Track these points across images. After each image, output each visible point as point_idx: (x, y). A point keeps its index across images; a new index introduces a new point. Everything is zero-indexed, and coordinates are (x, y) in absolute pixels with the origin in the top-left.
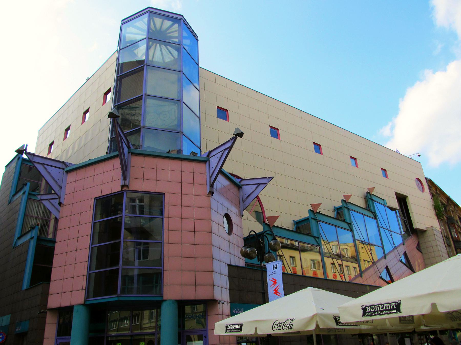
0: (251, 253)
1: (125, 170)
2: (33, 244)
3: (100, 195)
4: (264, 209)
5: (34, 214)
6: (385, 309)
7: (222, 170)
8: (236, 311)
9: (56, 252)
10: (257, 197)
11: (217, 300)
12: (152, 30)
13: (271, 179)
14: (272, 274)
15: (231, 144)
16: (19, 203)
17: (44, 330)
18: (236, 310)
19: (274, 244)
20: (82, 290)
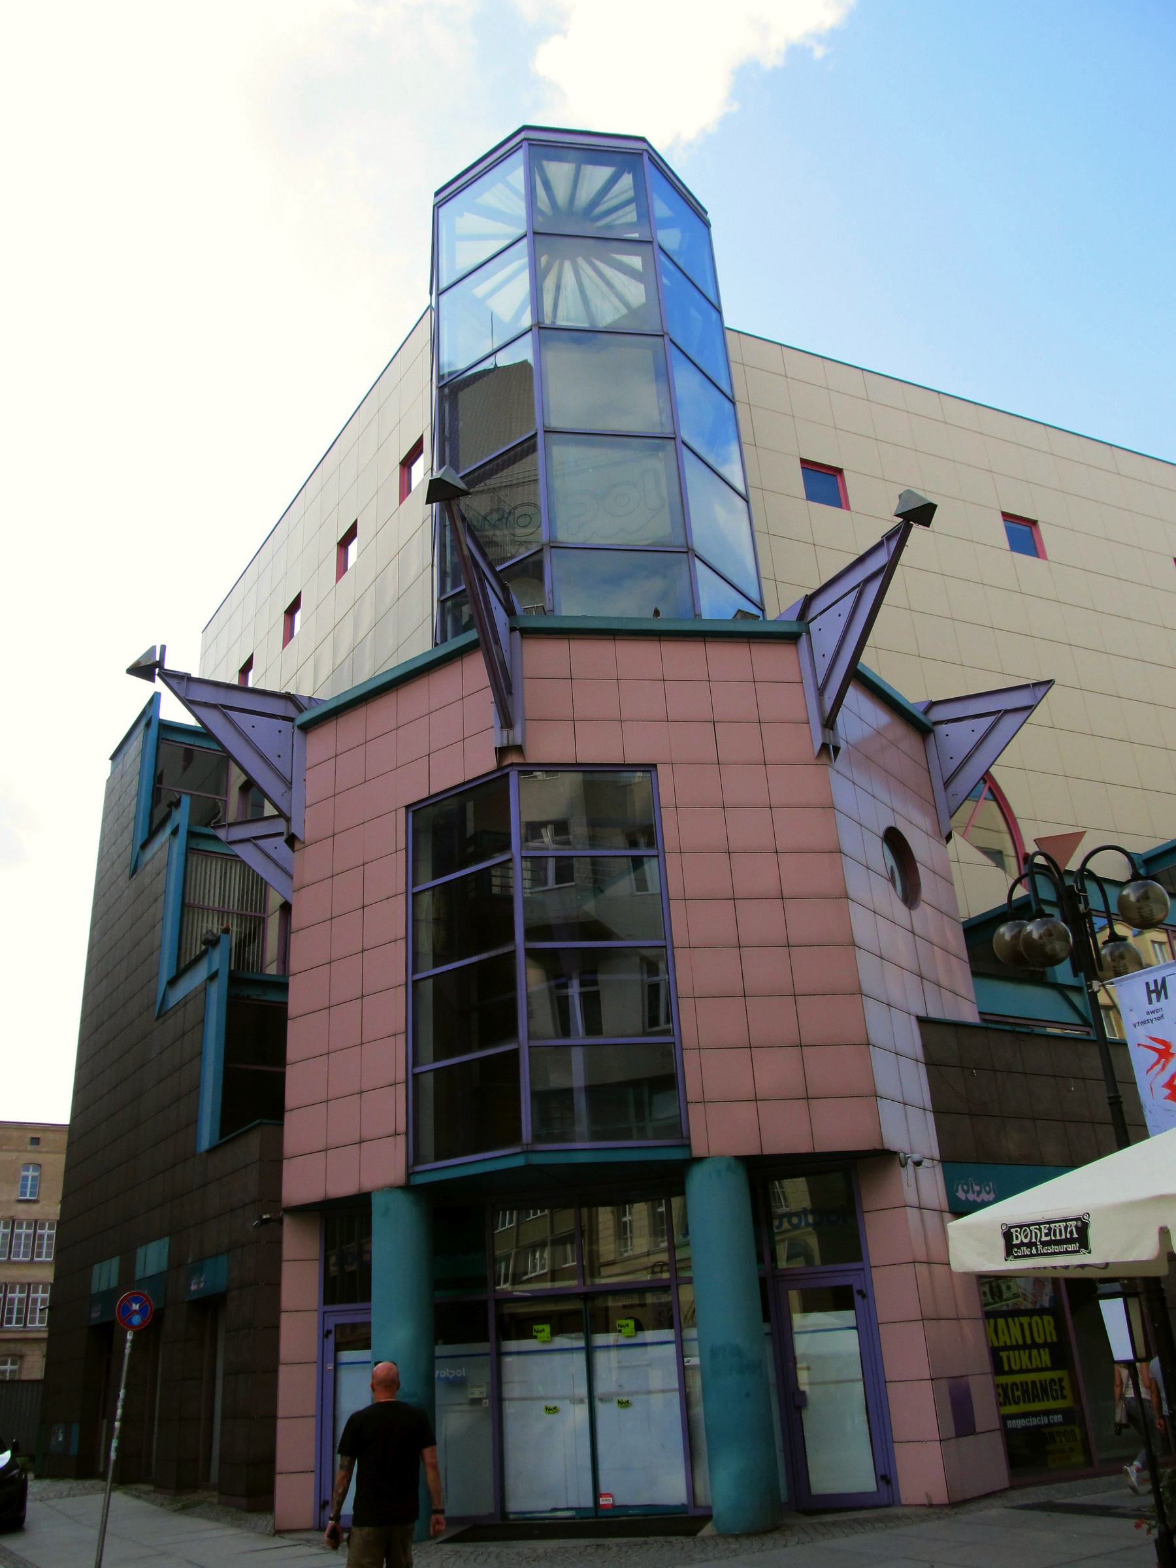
0: (1045, 939)
1: (505, 692)
2: (217, 994)
3: (425, 795)
4: (1014, 819)
5: (214, 902)
6: (1053, 1238)
7: (859, 667)
8: (966, 1192)
9: (292, 1010)
10: (987, 778)
11: (892, 1149)
12: (542, 213)
13: (1043, 689)
14: (1143, 1023)
15: (889, 555)
16: (164, 868)
17: (277, 1285)
18: (965, 1187)
19: (1138, 900)
20: (396, 1134)
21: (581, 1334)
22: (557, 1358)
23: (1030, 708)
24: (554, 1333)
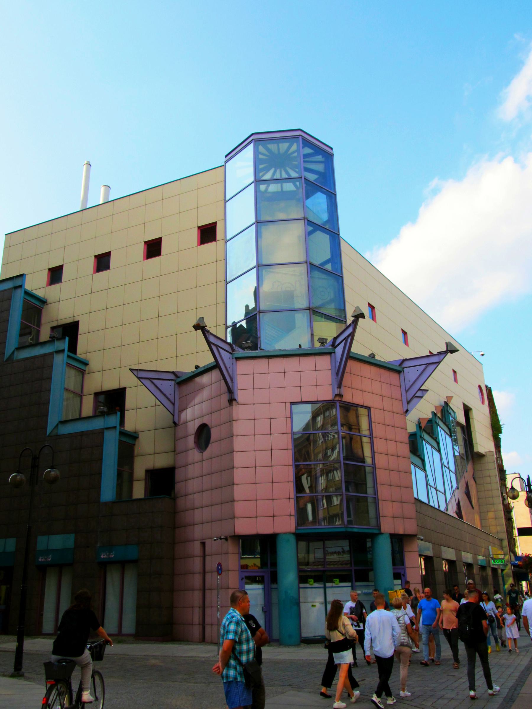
20: (290, 515)
21: (323, 583)
22: (314, 590)
23: (438, 363)
24: (315, 582)
